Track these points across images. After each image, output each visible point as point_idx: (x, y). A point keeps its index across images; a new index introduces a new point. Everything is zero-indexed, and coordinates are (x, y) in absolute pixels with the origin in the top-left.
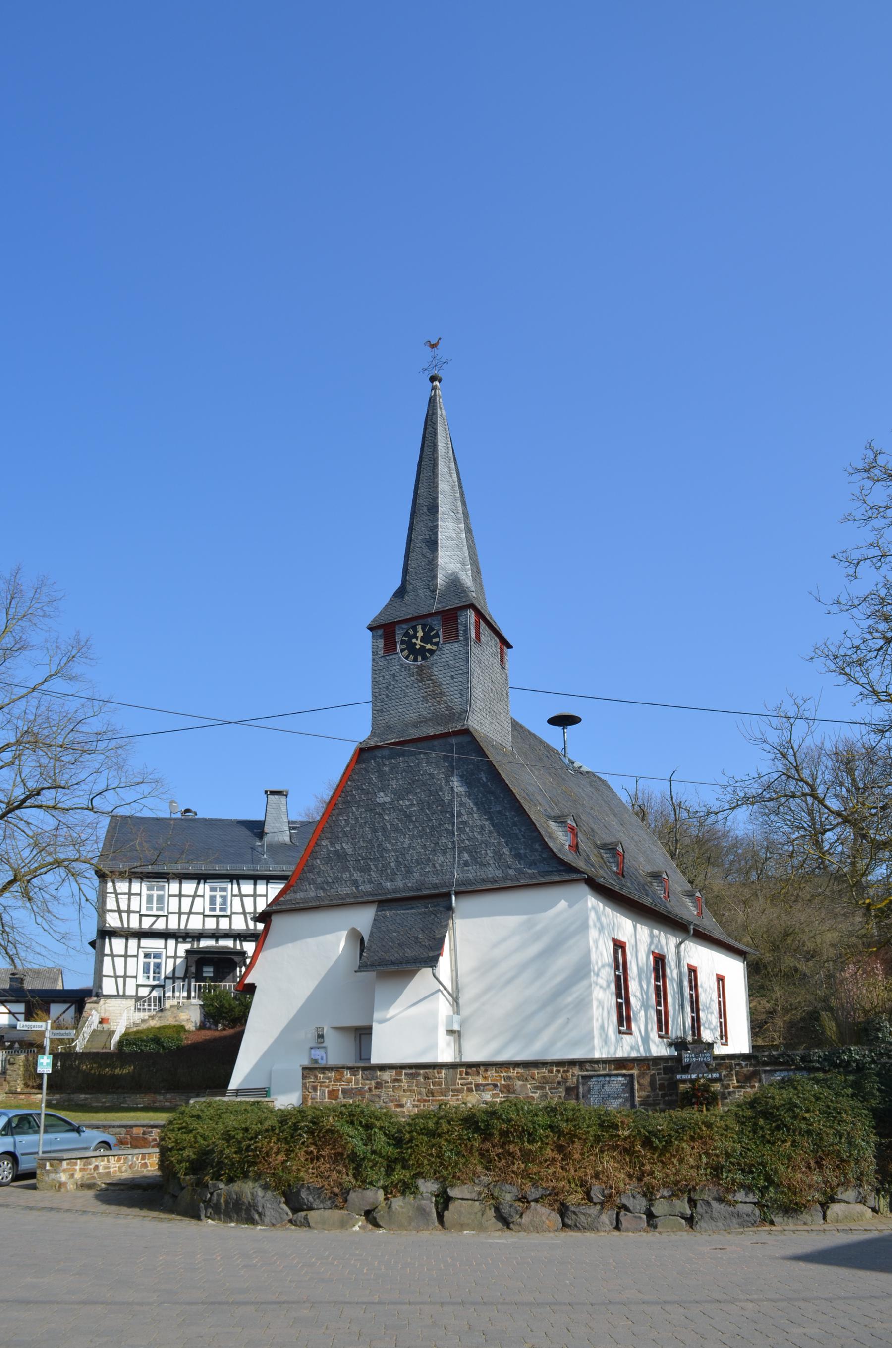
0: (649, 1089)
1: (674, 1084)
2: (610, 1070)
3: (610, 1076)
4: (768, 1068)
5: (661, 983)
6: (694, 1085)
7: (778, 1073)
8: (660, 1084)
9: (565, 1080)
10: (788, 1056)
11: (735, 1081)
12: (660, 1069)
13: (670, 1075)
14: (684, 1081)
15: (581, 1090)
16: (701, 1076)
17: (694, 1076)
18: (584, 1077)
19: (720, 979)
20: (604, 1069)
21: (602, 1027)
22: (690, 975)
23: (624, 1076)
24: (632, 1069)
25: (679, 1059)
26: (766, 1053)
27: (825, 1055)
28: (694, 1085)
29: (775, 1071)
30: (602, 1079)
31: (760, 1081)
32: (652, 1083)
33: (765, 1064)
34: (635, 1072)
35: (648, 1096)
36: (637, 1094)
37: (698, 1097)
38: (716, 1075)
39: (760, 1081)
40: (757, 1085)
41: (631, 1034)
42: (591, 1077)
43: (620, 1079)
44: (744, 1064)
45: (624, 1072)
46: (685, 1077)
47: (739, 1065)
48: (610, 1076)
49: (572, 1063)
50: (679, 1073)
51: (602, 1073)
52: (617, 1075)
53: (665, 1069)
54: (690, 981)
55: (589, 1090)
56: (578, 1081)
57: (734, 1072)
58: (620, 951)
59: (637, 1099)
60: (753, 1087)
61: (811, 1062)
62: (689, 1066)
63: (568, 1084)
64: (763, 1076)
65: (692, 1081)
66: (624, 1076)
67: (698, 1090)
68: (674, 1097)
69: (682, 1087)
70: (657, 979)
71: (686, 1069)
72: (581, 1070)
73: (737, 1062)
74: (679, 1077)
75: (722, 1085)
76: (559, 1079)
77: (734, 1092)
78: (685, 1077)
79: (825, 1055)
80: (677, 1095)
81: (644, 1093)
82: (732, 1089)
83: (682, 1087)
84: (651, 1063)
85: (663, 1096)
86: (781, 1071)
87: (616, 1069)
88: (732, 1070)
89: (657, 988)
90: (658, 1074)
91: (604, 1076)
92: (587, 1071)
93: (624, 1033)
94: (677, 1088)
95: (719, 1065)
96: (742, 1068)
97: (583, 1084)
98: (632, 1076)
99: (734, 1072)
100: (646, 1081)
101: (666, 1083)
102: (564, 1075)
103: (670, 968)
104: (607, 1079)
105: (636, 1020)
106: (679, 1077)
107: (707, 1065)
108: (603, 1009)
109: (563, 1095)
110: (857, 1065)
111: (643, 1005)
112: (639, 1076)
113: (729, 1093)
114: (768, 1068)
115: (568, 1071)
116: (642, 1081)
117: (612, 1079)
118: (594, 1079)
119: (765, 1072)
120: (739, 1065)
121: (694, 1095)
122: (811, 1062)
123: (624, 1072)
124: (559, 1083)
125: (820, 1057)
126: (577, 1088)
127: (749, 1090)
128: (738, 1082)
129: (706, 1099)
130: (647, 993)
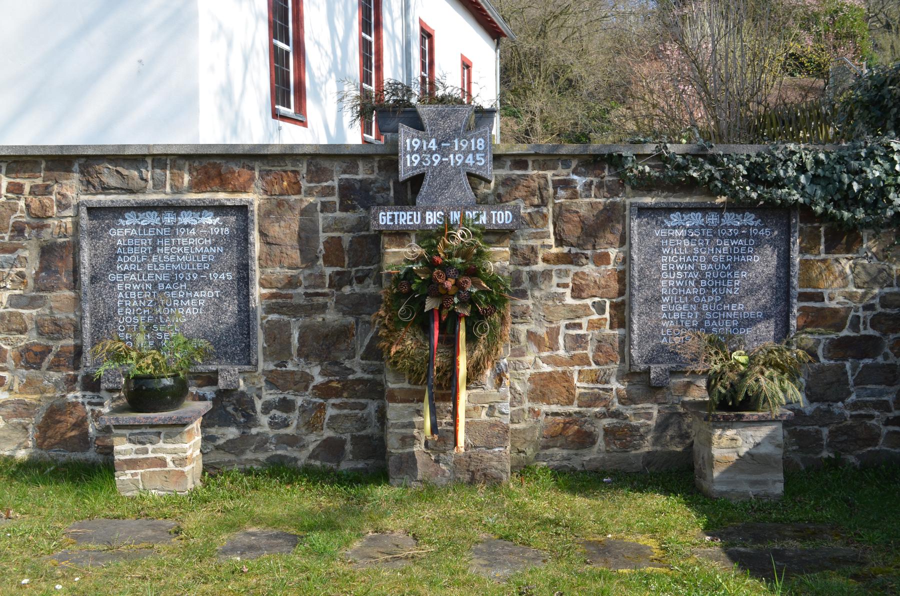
0: (296, 256)
1: (370, 244)
2: (176, 190)
3: (177, 208)
4: (649, 200)
5: (372, 39)
6: (432, 249)
7: (675, 218)
8: (328, 242)
9: (39, 219)
10: (713, 160)
11: (551, 241)
12: (329, 191)
13: (361, 212)
14: (400, 235)
15: (85, 257)
16: (455, 216)
17: (433, 218)
18: (93, 211)
19: (466, 66)
20: (159, 186)
21: (226, 91)
22: (422, 43)
23: (220, 209)
24: (244, 190)
25: (389, 160)
26: (650, 149)
27: (818, 162)
28: (432, 249)
29: (669, 210)
30: (151, 218)
31: (624, 240)
32: (306, 238)
33: (645, 185)
34: (254, 198)
35: (292, 283)
36: (257, 274)
37: (444, 296)
38: (502, 217)
39: (624, 240)
40: (613, 252)
41: (304, 124)
42: (119, 211)
43: (209, 219)
44: (580, 181)
45: (222, 196)
46: (406, 218)
47: (566, 184)
48: (177, 208)
49: (60, 161)
50: (385, 204)
51: (152, 197)
52: (198, 208)
53: (346, 189)
54: (423, 52)
55: (113, 259)
56: (76, 225)
57: (549, 210)
58: (340, 67)
59: (257, 292)
60: (602, 259)
61: (778, 183)
62: (417, 181)
63: (46, 235)
64: (635, 224)
65: (427, 236)
66: (220, 209)
67: (445, 267)
68: (371, 288)
69: (397, 256)
70: (365, 26)
71: (409, 191)
72: (88, 186)
73: (562, 173)
74: (384, 218)
75: (514, 250)
76: (21, 216)
77: (547, 274)
78: (406, 218)
79: (818, 162)
80: (378, 281)
81: (280, 272)
82: (540, 266)
83: (397, 256)
84: (303, 169)
85: (339, 281)
86: (684, 209)
87: (196, 186)
88: (544, 203)
89: (365, 45)
90: (325, 207)
91: (161, 208)
92: (106, 189)
93: (284, 118)
94: (377, 255)
95: (507, 182)
96: (575, 195)
97: (94, 235)
98: (242, 210)
99: (549, 210)
100: (286, 230)
101: (347, 238)
102: (35, 202)
103: (391, 13)
104: (169, 219)
105: (318, 99)
106: (384, 218)
107: (475, 178)
108: (230, 44)
109: (31, 269)
110: (115, 269)
111: (333, 69)
112: (266, 214)
113: (533, 277)
114: (649, 200)
115: (46, 190)
116: (276, 230)
117: (186, 218)
118: (130, 219)
119: (642, 210)
120: (566, 184)
121: (432, 288)
122: (778, 183)
123: (222, 196)
124: (18, 230)
125: (801, 169)
126: (76, 248)
127: (589, 268)
128: (560, 242)
129: (471, 300)
130: (344, 46)
